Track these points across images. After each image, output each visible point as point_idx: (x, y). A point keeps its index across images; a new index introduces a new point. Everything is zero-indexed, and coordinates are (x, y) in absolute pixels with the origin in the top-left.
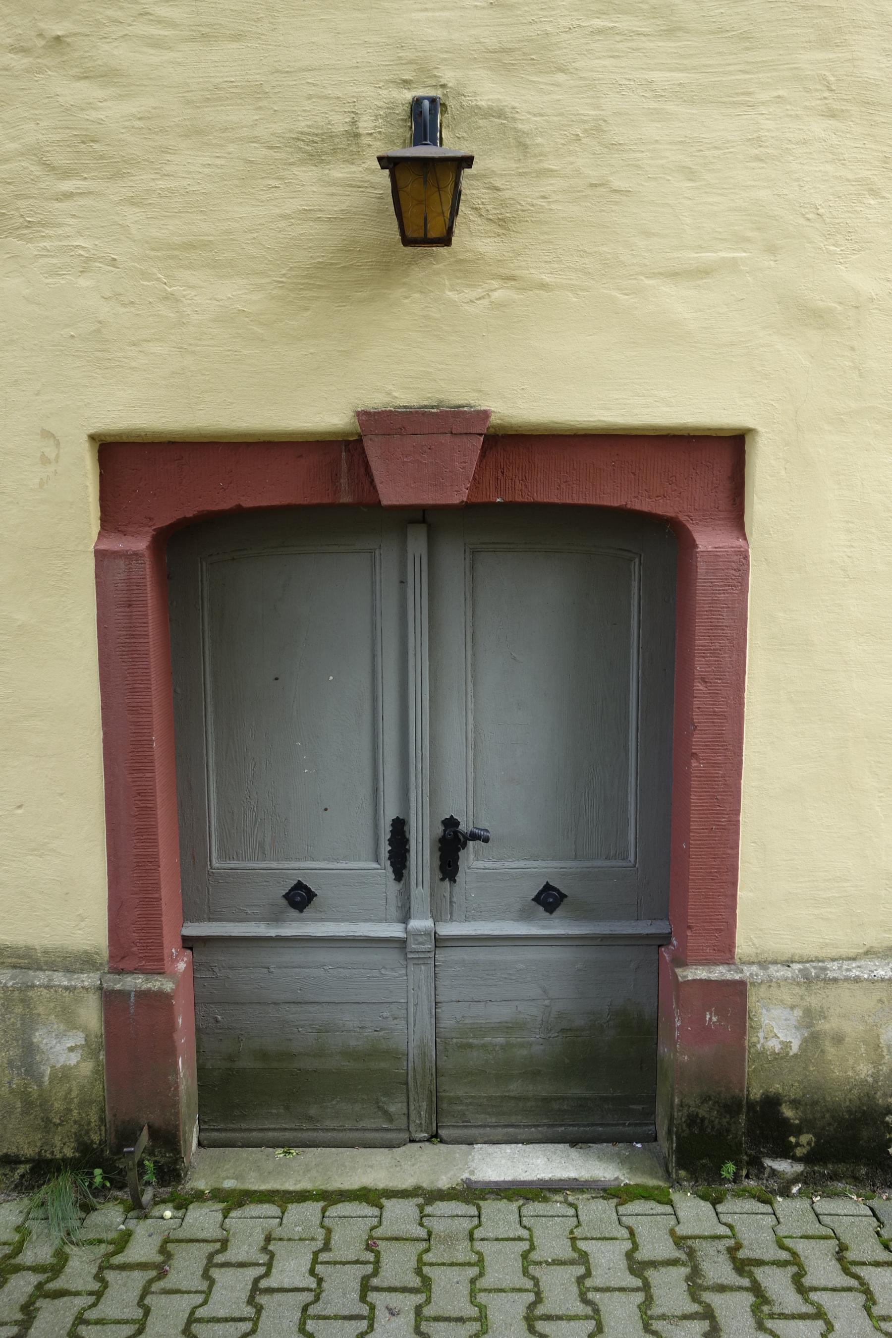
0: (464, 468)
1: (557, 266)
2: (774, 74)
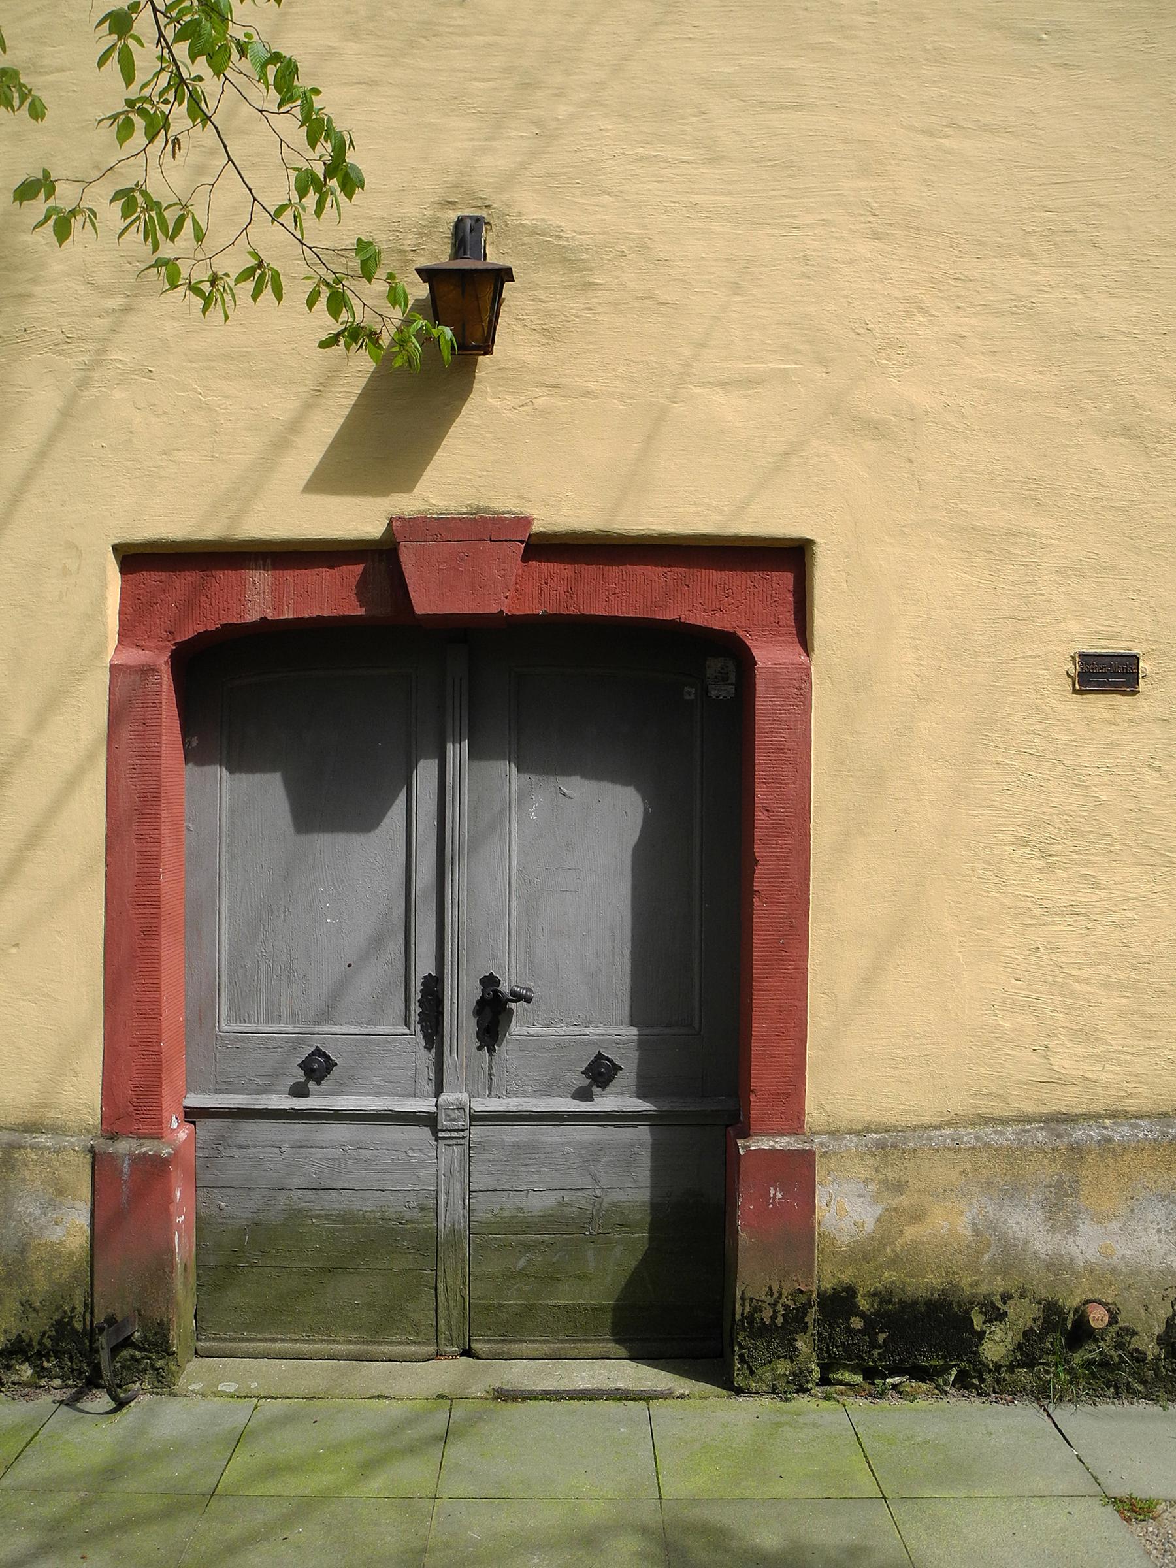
0: (503, 576)
1: (602, 374)
2: (818, 199)
